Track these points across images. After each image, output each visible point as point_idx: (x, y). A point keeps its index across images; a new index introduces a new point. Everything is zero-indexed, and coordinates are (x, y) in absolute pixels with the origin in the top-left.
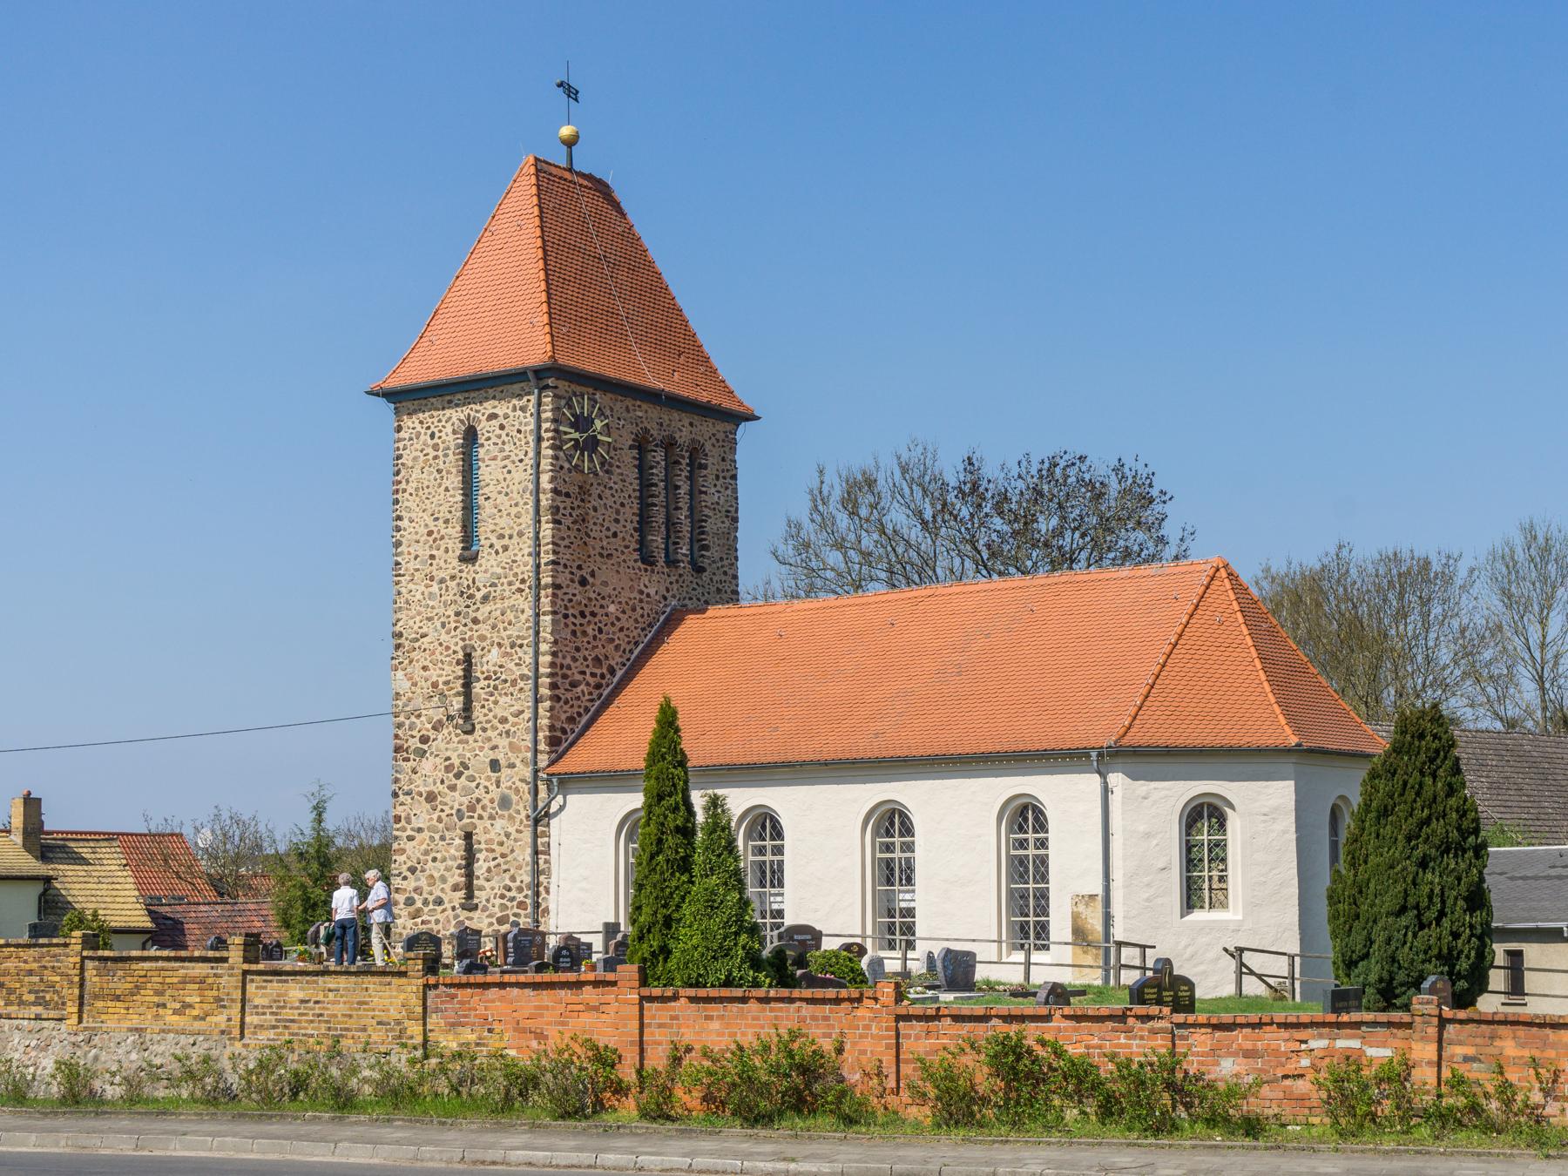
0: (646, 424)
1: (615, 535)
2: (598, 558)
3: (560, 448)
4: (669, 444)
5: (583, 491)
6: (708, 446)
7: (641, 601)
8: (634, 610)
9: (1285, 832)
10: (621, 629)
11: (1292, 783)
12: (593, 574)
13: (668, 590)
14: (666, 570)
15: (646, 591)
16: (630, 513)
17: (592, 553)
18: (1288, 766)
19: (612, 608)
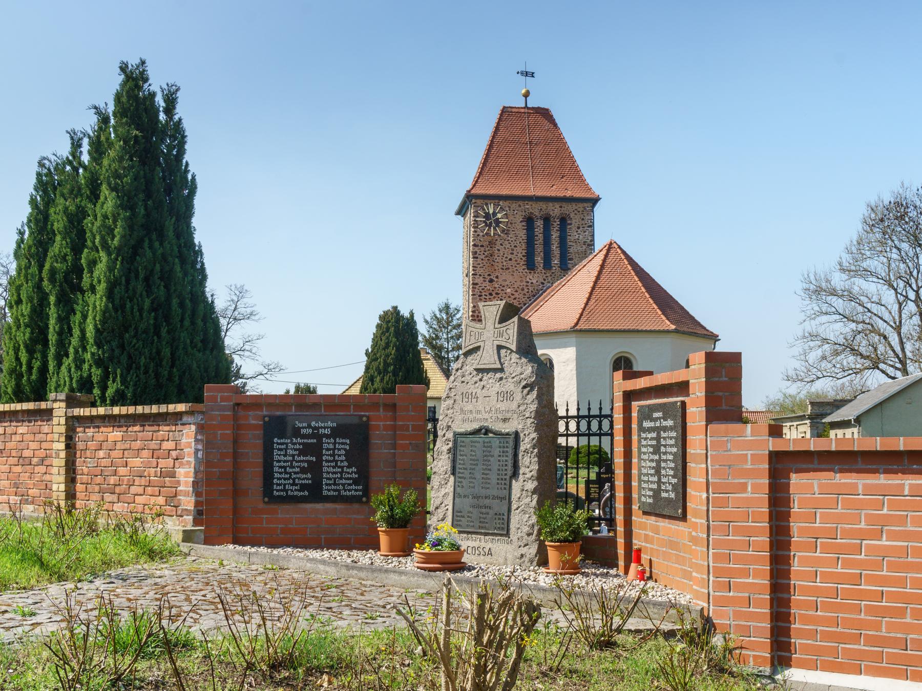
0: (531, 211)
1: (510, 259)
2: (500, 270)
3: (477, 227)
4: (547, 220)
5: (492, 243)
6: (572, 215)
7: (527, 286)
8: (523, 290)
9: (571, 370)
10: (515, 299)
11: (574, 349)
12: (497, 277)
13: (545, 280)
14: (543, 271)
15: (530, 281)
16: (521, 250)
17: (497, 268)
18: (573, 339)
19: (509, 290)
